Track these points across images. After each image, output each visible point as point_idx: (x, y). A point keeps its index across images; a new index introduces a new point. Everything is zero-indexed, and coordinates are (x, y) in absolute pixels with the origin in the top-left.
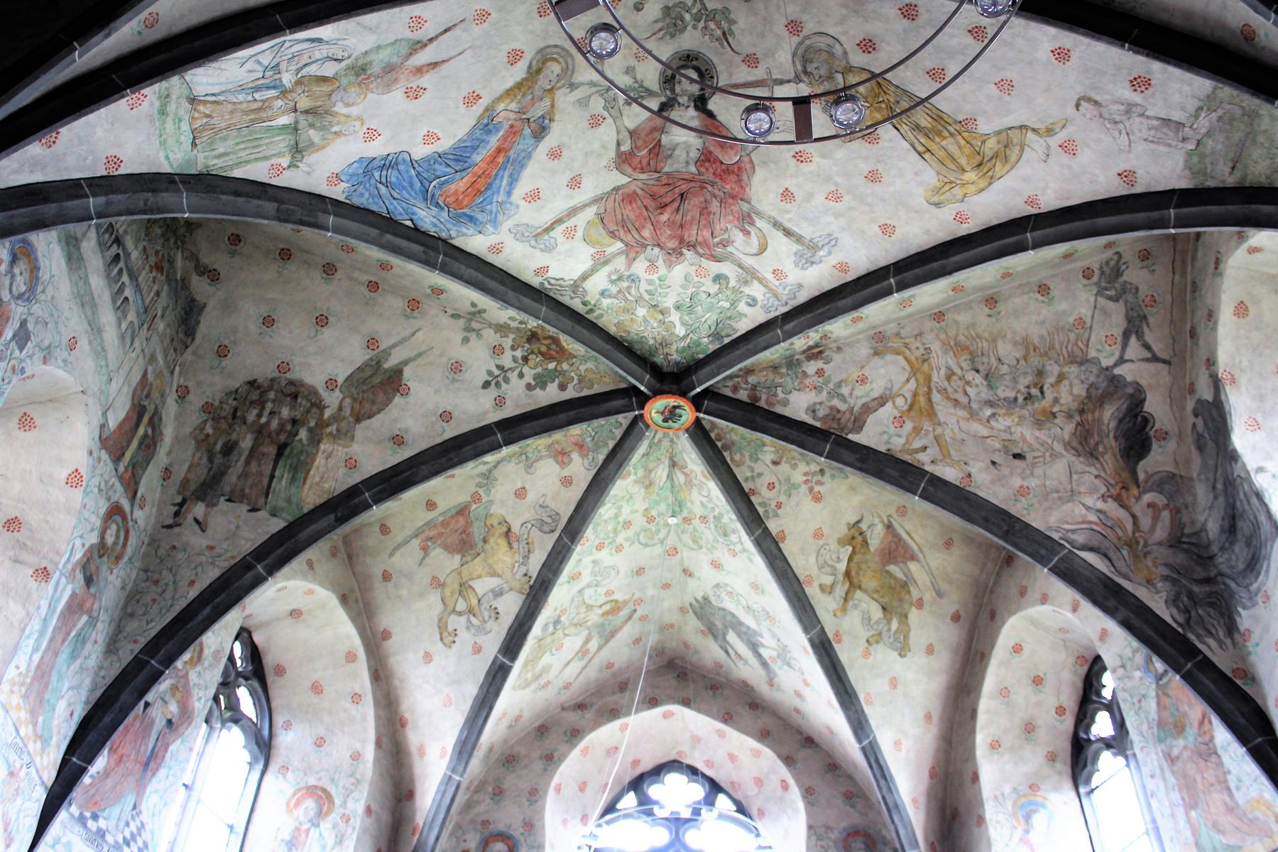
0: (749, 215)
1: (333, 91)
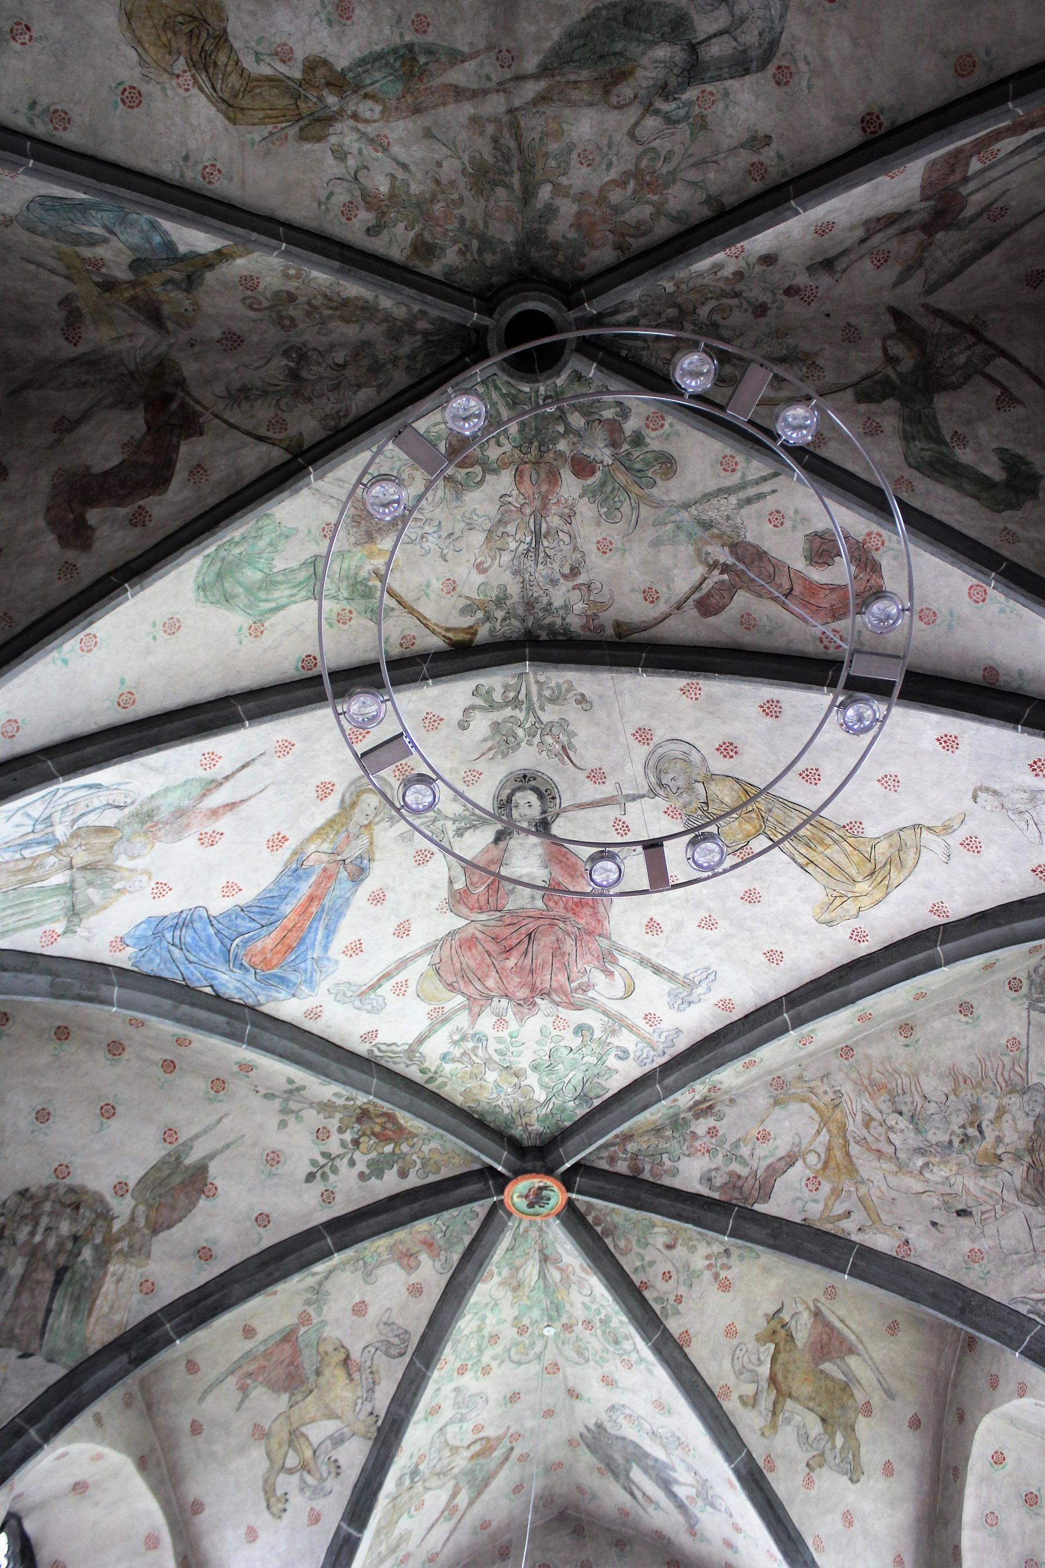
0: (610, 953)
1: (115, 843)
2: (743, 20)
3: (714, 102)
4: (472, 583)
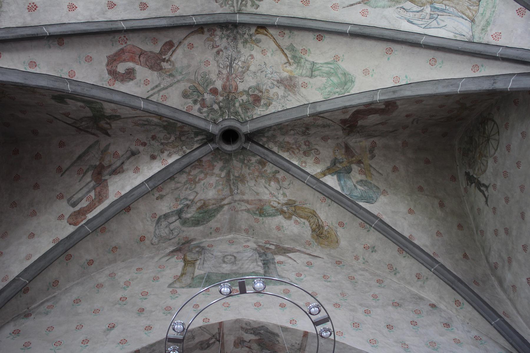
2: (166, 227)
3: (173, 206)
4: (256, 53)
